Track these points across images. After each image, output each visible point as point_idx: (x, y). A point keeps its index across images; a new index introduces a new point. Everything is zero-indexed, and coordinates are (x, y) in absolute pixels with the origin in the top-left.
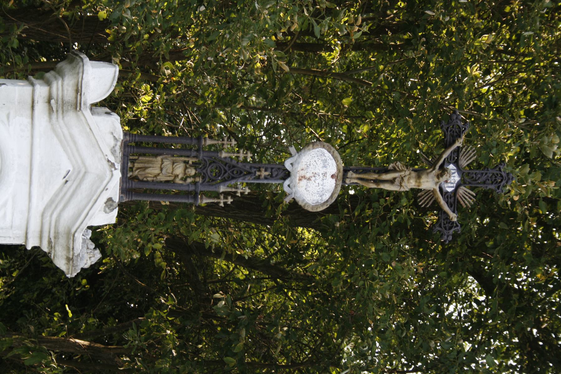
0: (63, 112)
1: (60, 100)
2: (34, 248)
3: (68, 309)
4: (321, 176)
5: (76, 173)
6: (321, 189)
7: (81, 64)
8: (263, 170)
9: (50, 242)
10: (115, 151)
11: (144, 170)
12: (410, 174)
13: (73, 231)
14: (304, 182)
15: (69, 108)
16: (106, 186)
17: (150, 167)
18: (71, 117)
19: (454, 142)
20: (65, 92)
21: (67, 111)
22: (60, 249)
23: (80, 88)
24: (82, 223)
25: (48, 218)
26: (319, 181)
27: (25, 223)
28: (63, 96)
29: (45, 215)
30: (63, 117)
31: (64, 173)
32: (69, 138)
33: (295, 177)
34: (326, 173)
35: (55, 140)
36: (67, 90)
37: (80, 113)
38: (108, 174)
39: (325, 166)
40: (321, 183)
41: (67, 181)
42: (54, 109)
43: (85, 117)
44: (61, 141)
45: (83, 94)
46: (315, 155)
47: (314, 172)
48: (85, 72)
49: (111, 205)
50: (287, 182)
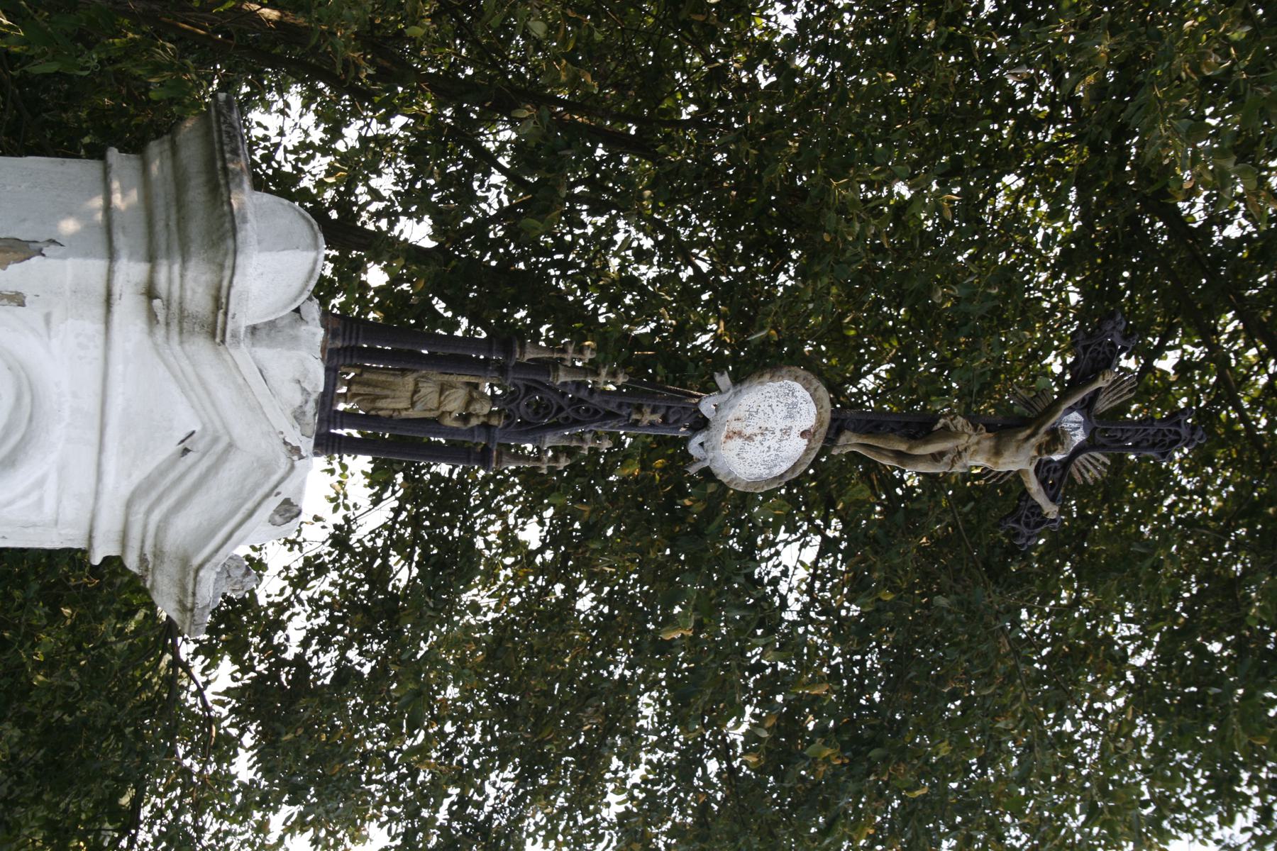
0: (181, 332)
2: (107, 560)
4: (778, 434)
5: (208, 439)
6: (773, 457)
7: (230, 242)
8: (647, 410)
9: (143, 560)
10: (304, 413)
12: (978, 443)
13: (196, 561)
14: (737, 443)
16: (276, 486)
17: (386, 397)
18: (200, 347)
19: (1095, 380)
20: (189, 294)
21: (192, 333)
22: (166, 581)
23: (224, 300)
24: (217, 550)
26: (772, 441)
27: (89, 516)
29: (135, 509)
30: (181, 343)
31: (183, 437)
32: (193, 379)
33: (718, 434)
34: (790, 428)
36: (194, 292)
37: (222, 347)
38: (284, 465)
39: (790, 416)
40: (774, 444)
41: (186, 451)
42: (161, 318)
44: (175, 376)
45: (230, 315)
46: (772, 394)
47: (764, 426)
48: (238, 272)
49: (287, 511)
50: (699, 438)
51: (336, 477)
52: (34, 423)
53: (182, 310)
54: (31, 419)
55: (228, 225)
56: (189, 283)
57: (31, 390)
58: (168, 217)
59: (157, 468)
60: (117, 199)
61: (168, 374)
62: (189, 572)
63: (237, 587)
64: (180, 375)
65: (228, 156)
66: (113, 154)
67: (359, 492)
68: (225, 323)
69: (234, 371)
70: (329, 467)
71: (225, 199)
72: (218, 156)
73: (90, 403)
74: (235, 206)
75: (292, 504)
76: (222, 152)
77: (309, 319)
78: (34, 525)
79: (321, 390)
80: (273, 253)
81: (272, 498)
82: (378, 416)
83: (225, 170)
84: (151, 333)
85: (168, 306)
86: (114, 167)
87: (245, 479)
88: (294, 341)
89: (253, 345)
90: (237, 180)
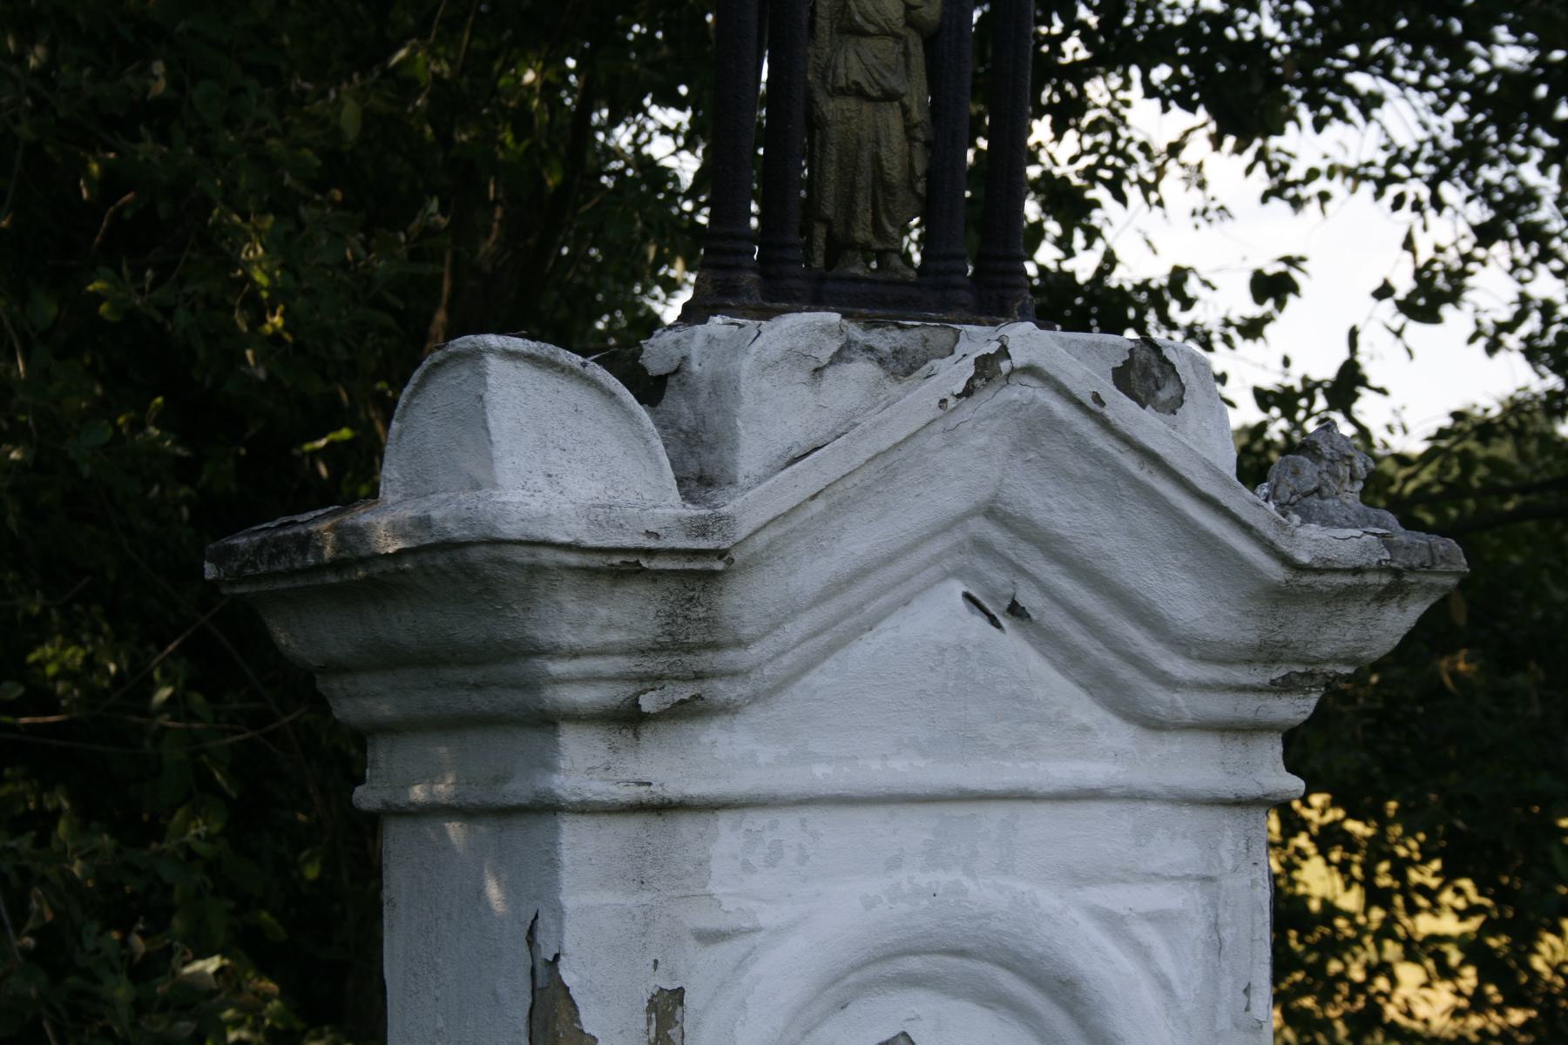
0: (715, 646)
1: (651, 665)
3: (322, 443)
5: (981, 564)
7: (475, 554)
9: (1285, 686)
10: (898, 353)
11: (888, 188)
13: (1275, 571)
15: (701, 612)
16: (1080, 405)
17: (876, 159)
18: (746, 602)
20: (614, 637)
21: (711, 623)
22: (1333, 633)
23: (617, 560)
24: (1246, 528)
25: (1180, 699)
27: (1187, 811)
28: (628, 651)
30: (740, 643)
31: (980, 621)
32: (832, 608)
35: (815, 679)
36: (609, 625)
37: (738, 556)
41: (1015, 610)
42: (686, 692)
43: (756, 532)
44: (830, 650)
45: (651, 544)
48: (540, 532)
49: (1146, 373)
51: (1337, 187)
52: (968, 945)
53: (658, 649)
54: (961, 953)
55: (441, 561)
56: (592, 637)
57: (889, 957)
58: (462, 684)
59: (1062, 670)
60: (444, 790)
61: (830, 664)
62: (1304, 586)
63: (1344, 471)
64: (825, 638)
65: (311, 560)
66: (367, 797)
67: (1354, 141)
68: (673, 552)
69: (795, 522)
70: (1316, 203)
71: (391, 566)
72: (316, 581)
73: (915, 827)
74: (400, 545)
75: (1128, 364)
76: (307, 571)
77: (677, 354)
78: (1215, 926)
79: (835, 317)
80: (496, 453)
81: (1109, 413)
82: (928, 174)
83: (338, 565)
84: (728, 709)
85: (655, 680)
86: (386, 795)
87: (1070, 476)
88: (724, 387)
89: (733, 482)
90: (352, 539)
